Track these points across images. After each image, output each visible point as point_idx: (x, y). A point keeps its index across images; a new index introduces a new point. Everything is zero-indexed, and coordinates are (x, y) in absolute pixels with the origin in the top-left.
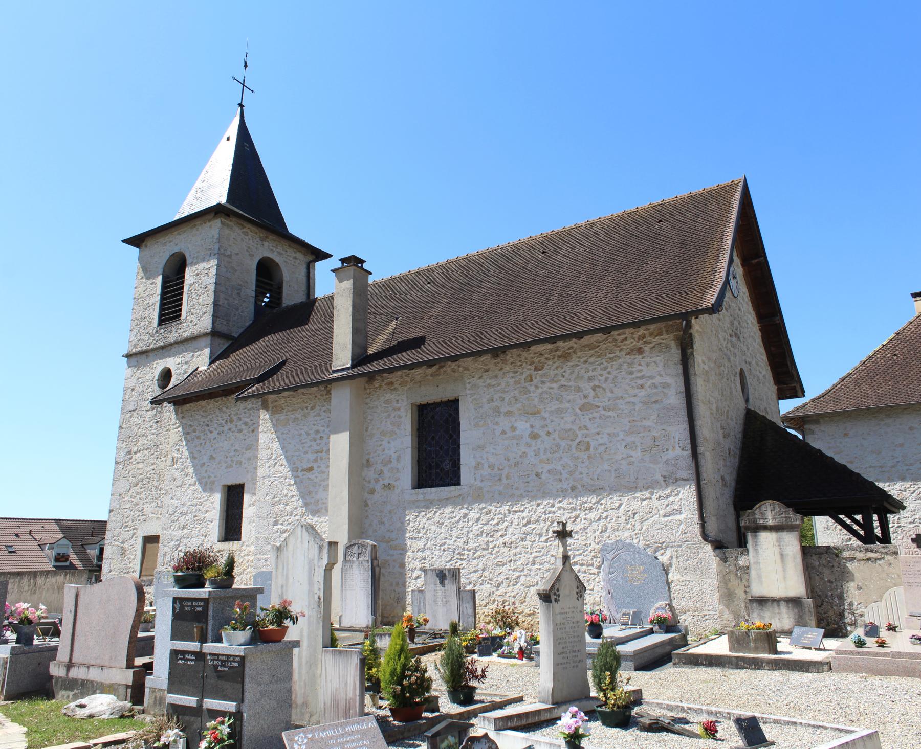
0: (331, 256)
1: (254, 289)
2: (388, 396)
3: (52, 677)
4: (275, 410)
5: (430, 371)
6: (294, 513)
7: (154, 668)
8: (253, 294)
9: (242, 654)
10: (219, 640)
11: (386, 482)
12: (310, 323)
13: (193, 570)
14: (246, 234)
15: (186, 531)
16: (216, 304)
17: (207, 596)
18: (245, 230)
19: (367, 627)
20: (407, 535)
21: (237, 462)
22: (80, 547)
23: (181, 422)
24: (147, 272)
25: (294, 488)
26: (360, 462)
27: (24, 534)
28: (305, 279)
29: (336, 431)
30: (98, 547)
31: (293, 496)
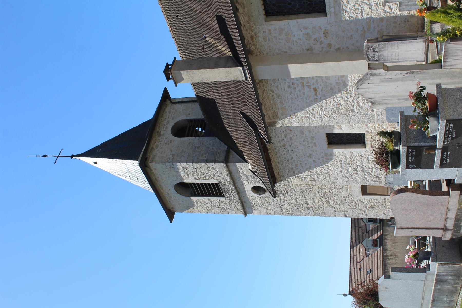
0: (165, 88)
1: (194, 138)
2: (261, 39)
3: (451, 238)
4: (276, 117)
5: (241, 10)
6: (346, 98)
7: (450, 179)
8: (197, 138)
9: (445, 122)
10: (435, 137)
11: (322, 36)
12: (213, 98)
13: (387, 158)
14: (157, 146)
15: (358, 169)
16: (207, 162)
17: (406, 147)
18: (155, 147)
19: (425, 42)
20: (360, 18)
21: (312, 140)
22: (368, 233)
23: (287, 178)
24: (189, 206)
25: (328, 100)
26: (309, 56)
27: (359, 265)
28: (183, 105)
29: (288, 73)
30: (367, 223)
31: (334, 100)
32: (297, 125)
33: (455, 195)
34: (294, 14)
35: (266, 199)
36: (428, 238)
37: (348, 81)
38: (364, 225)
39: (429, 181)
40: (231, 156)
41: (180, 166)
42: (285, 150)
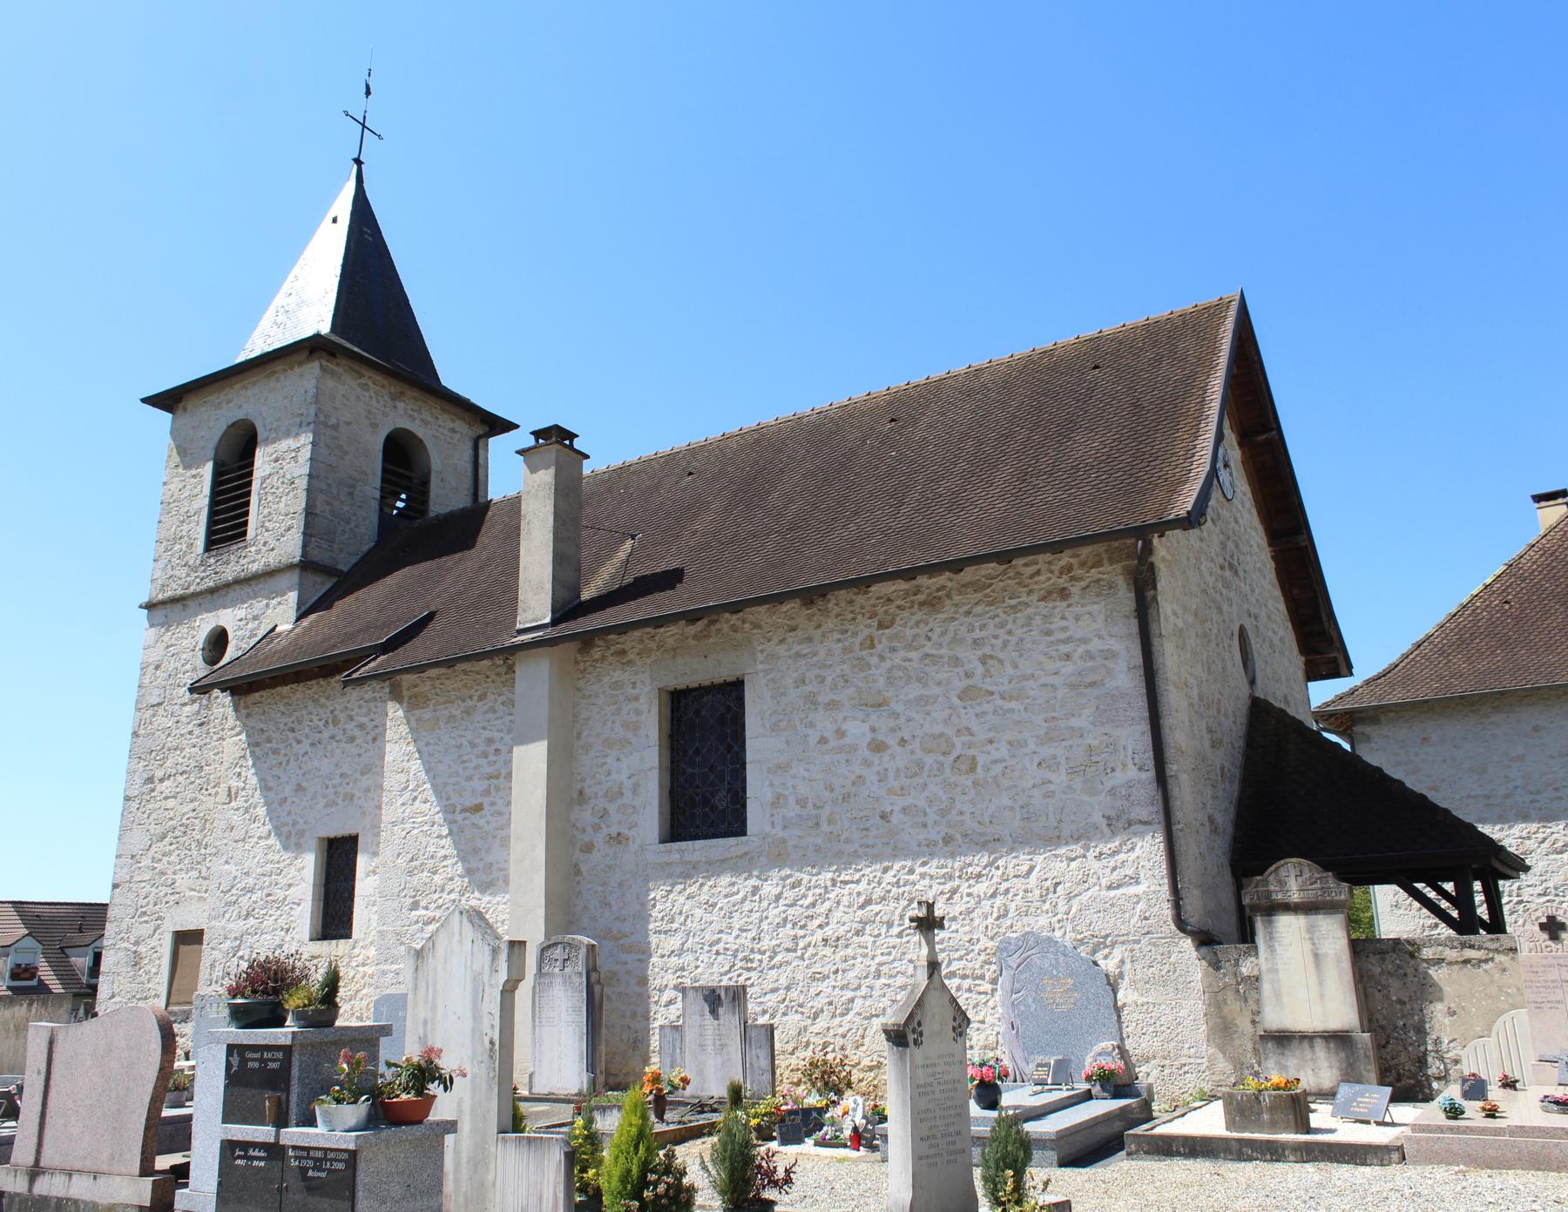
2: (617, 675)
4: (414, 703)
5: (692, 630)
8: (377, 494)
9: (352, 1147)
10: (310, 1121)
11: (614, 830)
12: (479, 545)
13: (263, 993)
14: (365, 387)
15: (252, 921)
16: (309, 512)
17: (289, 1042)
18: (363, 381)
20: (651, 926)
21: (345, 796)
23: (245, 725)
24: (186, 454)
25: (447, 842)
26: (566, 794)
28: (469, 467)
29: (523, 740)
30: (90, 951)
31: (445, 857)
32: (388, 758)
33: (143, 1191)
34: (672, 762)
35: (188, 666)
36: (13, 1124)
37: (494, 894)
38: (87, 941)
39: (189, 1118)
40: (319, 579)
41: (303, 443)
42: (321, 724)
